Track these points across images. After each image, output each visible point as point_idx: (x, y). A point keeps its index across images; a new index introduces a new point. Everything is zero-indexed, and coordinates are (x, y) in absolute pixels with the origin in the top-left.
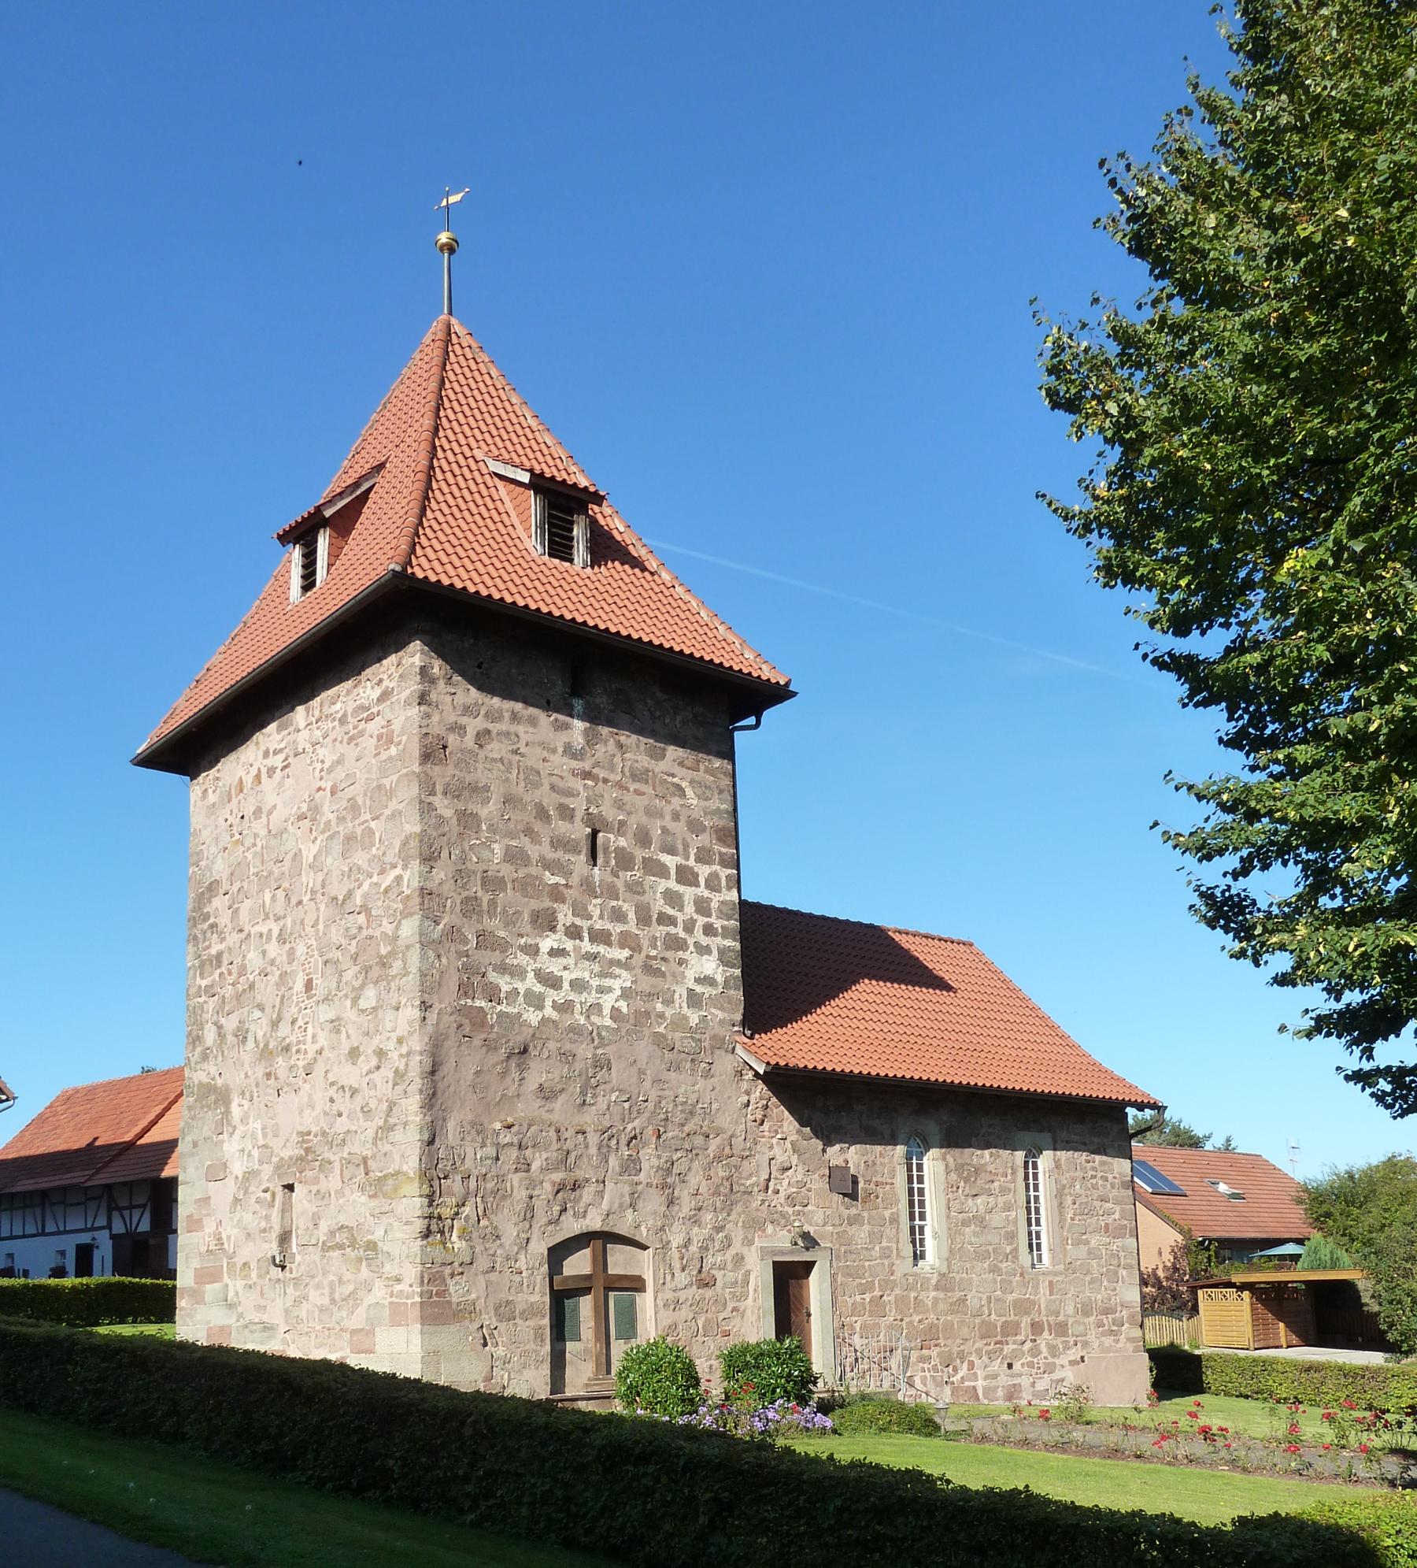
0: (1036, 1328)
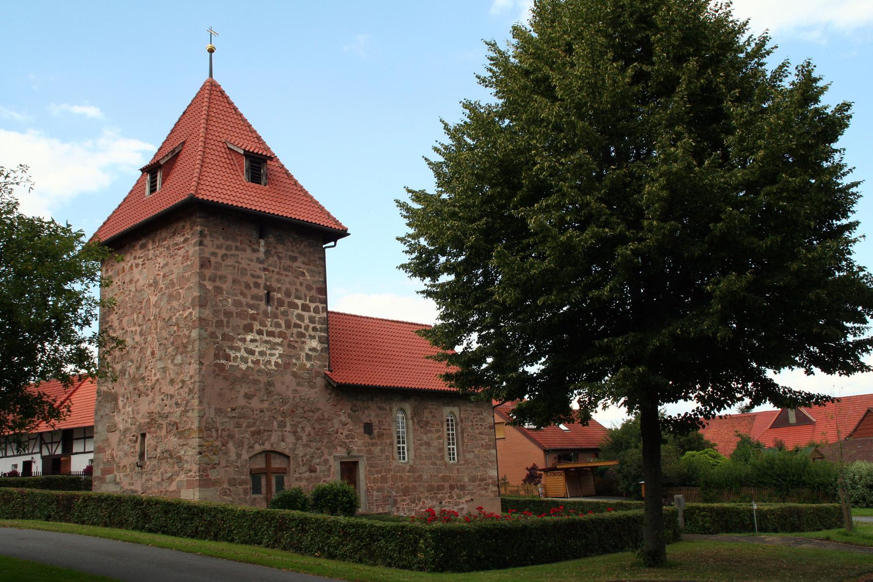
0: (452, 487)
